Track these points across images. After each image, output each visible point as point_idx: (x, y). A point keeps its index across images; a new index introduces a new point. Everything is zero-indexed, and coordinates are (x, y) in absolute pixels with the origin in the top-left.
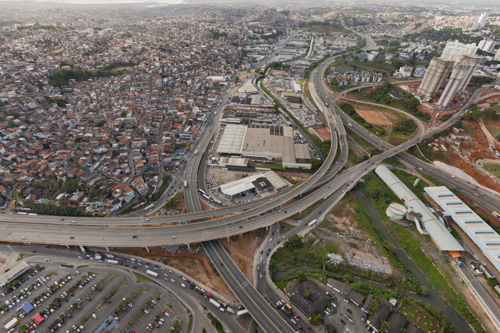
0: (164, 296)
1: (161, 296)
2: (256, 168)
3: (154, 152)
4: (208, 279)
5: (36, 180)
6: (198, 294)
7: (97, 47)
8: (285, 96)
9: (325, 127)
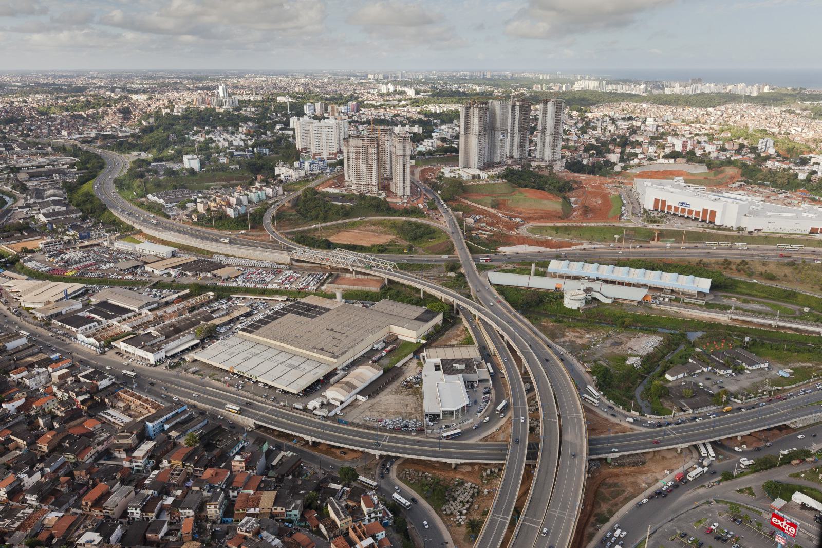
0: (679, 528)
1: (678, 531)
2: (399, 365)
3: (805, 113)
4: (649, 475)
5: (793, 168)
6: (675, 491)
7: (87, 168)
8: (173, 268)
9: (338, 276)
